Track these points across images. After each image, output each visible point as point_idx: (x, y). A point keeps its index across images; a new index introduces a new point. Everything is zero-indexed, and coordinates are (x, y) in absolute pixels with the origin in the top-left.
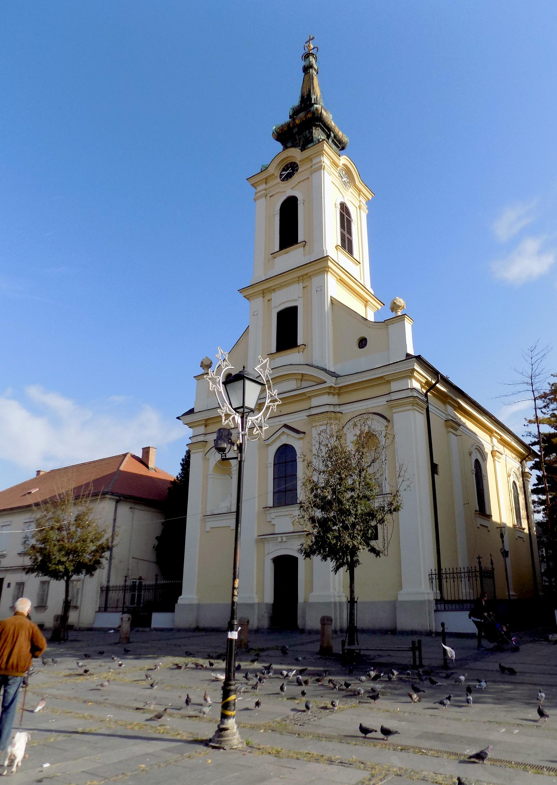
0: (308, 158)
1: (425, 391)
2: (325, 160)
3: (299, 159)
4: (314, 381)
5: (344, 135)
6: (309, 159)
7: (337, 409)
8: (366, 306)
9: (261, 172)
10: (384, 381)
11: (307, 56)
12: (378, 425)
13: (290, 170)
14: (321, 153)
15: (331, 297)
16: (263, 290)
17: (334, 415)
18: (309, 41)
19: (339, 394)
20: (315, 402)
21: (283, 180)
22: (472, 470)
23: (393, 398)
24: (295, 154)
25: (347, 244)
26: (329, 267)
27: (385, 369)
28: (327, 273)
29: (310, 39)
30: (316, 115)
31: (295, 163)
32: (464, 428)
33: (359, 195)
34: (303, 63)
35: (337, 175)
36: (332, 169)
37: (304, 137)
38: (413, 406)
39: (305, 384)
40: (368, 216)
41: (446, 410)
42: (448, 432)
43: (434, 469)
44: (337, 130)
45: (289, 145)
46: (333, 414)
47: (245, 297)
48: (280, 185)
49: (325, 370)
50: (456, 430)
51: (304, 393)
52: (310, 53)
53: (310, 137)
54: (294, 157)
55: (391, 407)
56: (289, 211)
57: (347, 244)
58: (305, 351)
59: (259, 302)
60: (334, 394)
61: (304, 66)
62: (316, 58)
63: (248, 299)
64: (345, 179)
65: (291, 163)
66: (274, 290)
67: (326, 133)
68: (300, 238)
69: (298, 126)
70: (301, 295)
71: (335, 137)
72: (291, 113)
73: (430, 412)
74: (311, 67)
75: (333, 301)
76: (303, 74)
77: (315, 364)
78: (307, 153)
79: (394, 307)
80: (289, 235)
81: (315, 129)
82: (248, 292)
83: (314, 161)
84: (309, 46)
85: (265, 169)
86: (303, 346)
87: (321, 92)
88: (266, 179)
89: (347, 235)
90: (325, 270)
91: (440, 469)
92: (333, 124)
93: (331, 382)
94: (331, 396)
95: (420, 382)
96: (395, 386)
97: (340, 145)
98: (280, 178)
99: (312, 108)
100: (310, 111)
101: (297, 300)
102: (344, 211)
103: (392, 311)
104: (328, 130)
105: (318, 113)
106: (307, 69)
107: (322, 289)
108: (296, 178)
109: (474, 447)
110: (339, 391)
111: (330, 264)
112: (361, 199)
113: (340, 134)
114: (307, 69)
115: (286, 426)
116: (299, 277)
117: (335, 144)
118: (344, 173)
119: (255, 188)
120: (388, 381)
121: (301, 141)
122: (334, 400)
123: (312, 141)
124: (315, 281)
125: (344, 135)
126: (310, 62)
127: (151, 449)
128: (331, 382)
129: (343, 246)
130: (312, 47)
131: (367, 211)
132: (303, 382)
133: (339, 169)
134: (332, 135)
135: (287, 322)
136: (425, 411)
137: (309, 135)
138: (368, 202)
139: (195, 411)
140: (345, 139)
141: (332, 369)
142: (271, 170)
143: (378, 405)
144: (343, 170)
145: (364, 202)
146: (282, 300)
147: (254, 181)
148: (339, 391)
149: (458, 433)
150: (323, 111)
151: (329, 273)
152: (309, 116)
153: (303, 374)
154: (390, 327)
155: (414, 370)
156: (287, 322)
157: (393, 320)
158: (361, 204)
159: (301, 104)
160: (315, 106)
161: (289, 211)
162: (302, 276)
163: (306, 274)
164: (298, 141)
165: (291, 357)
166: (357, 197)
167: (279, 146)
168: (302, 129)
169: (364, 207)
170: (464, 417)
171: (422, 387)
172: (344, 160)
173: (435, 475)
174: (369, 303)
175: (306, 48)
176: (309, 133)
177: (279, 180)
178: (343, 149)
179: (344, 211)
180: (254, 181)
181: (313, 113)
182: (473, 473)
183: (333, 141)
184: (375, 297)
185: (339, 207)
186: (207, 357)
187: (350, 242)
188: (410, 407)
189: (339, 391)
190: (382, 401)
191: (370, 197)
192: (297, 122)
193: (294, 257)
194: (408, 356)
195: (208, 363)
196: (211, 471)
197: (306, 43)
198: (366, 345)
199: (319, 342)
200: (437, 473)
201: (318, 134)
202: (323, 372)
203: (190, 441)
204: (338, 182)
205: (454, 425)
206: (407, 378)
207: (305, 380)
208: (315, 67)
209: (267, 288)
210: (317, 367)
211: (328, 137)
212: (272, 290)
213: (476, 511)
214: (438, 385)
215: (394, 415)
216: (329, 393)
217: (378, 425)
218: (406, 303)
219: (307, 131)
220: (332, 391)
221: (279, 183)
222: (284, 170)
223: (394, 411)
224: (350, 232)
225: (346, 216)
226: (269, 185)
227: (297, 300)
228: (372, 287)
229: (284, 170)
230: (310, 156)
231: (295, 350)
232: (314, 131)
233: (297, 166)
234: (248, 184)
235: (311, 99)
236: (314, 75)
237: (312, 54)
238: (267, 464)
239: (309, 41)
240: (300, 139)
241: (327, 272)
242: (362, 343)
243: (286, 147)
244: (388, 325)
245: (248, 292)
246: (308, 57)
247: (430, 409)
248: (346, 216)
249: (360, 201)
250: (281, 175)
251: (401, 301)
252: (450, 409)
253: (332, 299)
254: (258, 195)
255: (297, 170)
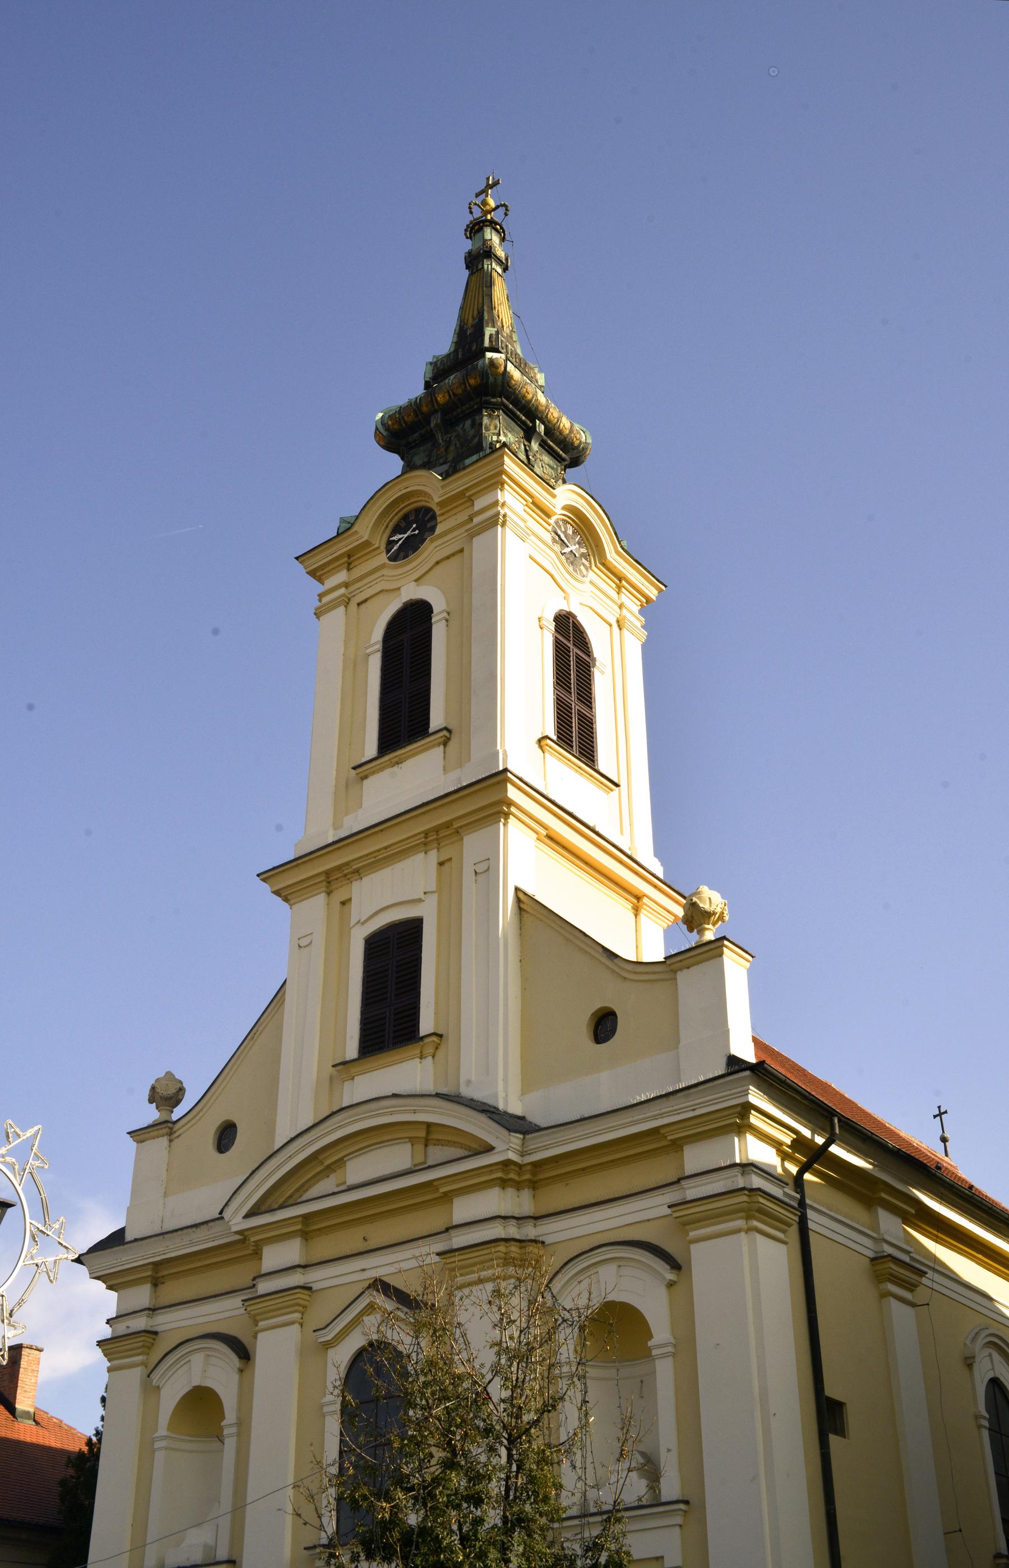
0: (462, 494)
1: (794, 1169)
2: (509, 499)
3: (437, 500)
4: (462, 1146)
5: (577, 427)
6: (465, 498)
7: (530, 1231)
8: (636, 911)
9: (338, 535)
10: (664, 1142)
11: (475, 229)
12: (641, 1288)
13: (412, 528)
14: (496, 480)
15: (517, 889)
16: (327, 873)
17: (520, 1253)
18: (484, 192)
19: (534, 1185)
20: (464, 1209)
21: (393, 558)
22: (977, 1417)
23: (691, 1194)
24: (431, 485)
25: (575, 732)
26: (510, 803)
27: (666, 1106)
28: (506, 819)
29: (490, 187)
30: (491, 379)
31: (428, 510)
32: (937, 1277)
33: (619, 588)
34: (468, 245)
35: (548, 537)
36: (532, 524)
37: (458, 436)
38: (748, 1218)
39: (437, 1154)
40: (647, 649)
41: (876, 1228)
42: (886, 1295)
43: (829, 1416)
44: (554, 413)
45: (418, 460)
46: (514, 1248)
47: (277, 893)
48: (385, 572)
49: (490, 1111)
50: (911, 1287)
51: (429, 1184)
52: (487, 220)
53: (474, 437)
54: (426, 494)
55: (685, 1225)
56: (408, 643)
57: (575, 732)
58: (440, 1053)
59: (316, 906)
60: (518, 1186)
61: (470, 253)
62: (502, 233)
63: (286, 900)
64: (573, 548)
65: (417, 511)
66: (357, 871)
67: (522, 425)
68: (437, 719)
69: (446, 410)
70: (433, 887)
71: (549, 432)
72: (429, 375)
73: (812, 1237)
74: (488, 253)
75: (526, 905)
76: (467, 273)
77: (466, 1092)
78: (460, 482)
79: (695, 917)
80: (404, 717)
81: (490, 416)
82: (287, 880)
83: (479, 504)
84: (485, 203)
85: (347, 527)
86: (435, 1039)
87: (516, 315)
88: (349, 556)
89: (576, 706)
90: (499, 810)
91: (853, 1417)
92: (542, 399)
93: (507, 1147)
94: (510, 1191)
95: (777, 1144)
96: (696, 1157)
97: (567, 455)
98: (388, 552)
99: (480, 362)
100: (475, 368)
101: (420, 900)
102: (570, 640)
103: (691, 930)
104: (526, 416)
105: (496, 375)
106: (477, 260)
107: (489, 869)
108: (431, 550)
109: (981, 1341)
110: (531, 1176)
111: (512, 793)
112: (626, 598)
113: (565, 423)
114: (477, 260)
115: (381, 1286)
116: (426, 834)
117: (551, 452)
118: (570, 532)
119: (321, 580)
120: (445, 1194)
121: (452, 448)
122: (521, 1202)
123: (479, 447)
124: (472, 843)
125: (577, 427)
126: (485, 241)
127: (25, 1352)
128: (507, 1147)
129: (564, 738)
130: (492, 203)
131: (644, 634)
132: (431, 1149)
133: (552, 521)
134: (541, 428)
135: (393, 963)
136: (794, 1231)
137: (472, 432)
138: (647, 606)
139: (129, 1236)
140: (582, 436)
141: (515, 1108)
142: (364, 531)
143: (224, 1313)
144: (565, 522)
145: (636, 609)
146: (381, 898)
147: (317, 562)
148: (531, 1176)
149: (921, 1295)
150: (510, 367)
151: (512, 820)
152: (472, 381)
153: (429, 1126)
154: (682, 977)
155: (748, 1108)
156: (393, 963)
157: (697, 954)
158: (625, 612)
159: (456, 351)
160: (489, 355)
161: (408, 643)
162: (437, 830)
163: (448, 825)
164: (442, 450)
165: (406, 1073)
166: (613, 594)
167: (394, 463)
168: (455, 418)
169: (635, 621)
170: (937, 1240)
171: (785, 1156)
172: (566, 495)
173: (833, 1438)
174: (645, 900)
175: (475, 209)
176: (473, 425)
177: (383, 558)
178: (575, 462)
179: (570, 640)
180: (317, 562)
181: (484, 374)
182: (980, 1427)
183: (543, 444)
184: (667, 884)
185: (552, 626)
186: (169, 1074)
187: (588, 726)
188: (740, 1223)
189: (534, 1174)
190: (657, 1205)
191: (653, 593)
192: (441, 398)
193: (420, 775)
194: (734, 1063)
195: (172, 1091)
196: (162, 1431)
197: (477, 195)
198: (613, 1032)
199: (488, 1035)
200: (841, 1431)
201: (499, 430)
202: (483, 1118)
203: (107, 1332)
204: (551, 557)
205: (903, 1274)
206: (732, 1131)
207: (439, 1142)
208: (500, 253)
209: (339, 868)
210: (472, 1104)
211: (529, 433)
212: (352, 872)
213: (998, 1556)
214: (834, 1149)
215: (693, 1247)
216: (504, 1183)
217: (641, 1288)
218: (730, 905)
219: (468, 423)
220: (512, 1176)
221: (383, 566)
222: (397, 529)
223: (692, 1234)
224: (586, 696)
225: (574, 651)
226: (357, 572)
227: (420, 900)
228: (657, 854)
229: (397, 529)
230: (467, 489)
231: (414, 1049)
232: (486, 421)
233: (434, 517)
234: (299, 569)
235: (483, 335)
236: (494, 274)
237: (492, 223)
238: (322, 1406)
239: (484, 192)
240: (448, 443)
241: (507, 815)
242: (604, 1025)
243: (409, 467)
244: (676, 972)
245: (287, 880)
246: (481, 229)
247: (811, 1225)
248: (574, 651)
249: (621, 607)
250: (390, 544)
251: (712, 899)
252: (888, 1223)
253: (521, 896)
254: (325, 600)
255: (433, 529)
